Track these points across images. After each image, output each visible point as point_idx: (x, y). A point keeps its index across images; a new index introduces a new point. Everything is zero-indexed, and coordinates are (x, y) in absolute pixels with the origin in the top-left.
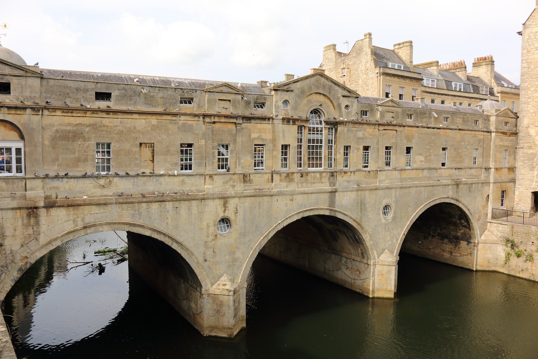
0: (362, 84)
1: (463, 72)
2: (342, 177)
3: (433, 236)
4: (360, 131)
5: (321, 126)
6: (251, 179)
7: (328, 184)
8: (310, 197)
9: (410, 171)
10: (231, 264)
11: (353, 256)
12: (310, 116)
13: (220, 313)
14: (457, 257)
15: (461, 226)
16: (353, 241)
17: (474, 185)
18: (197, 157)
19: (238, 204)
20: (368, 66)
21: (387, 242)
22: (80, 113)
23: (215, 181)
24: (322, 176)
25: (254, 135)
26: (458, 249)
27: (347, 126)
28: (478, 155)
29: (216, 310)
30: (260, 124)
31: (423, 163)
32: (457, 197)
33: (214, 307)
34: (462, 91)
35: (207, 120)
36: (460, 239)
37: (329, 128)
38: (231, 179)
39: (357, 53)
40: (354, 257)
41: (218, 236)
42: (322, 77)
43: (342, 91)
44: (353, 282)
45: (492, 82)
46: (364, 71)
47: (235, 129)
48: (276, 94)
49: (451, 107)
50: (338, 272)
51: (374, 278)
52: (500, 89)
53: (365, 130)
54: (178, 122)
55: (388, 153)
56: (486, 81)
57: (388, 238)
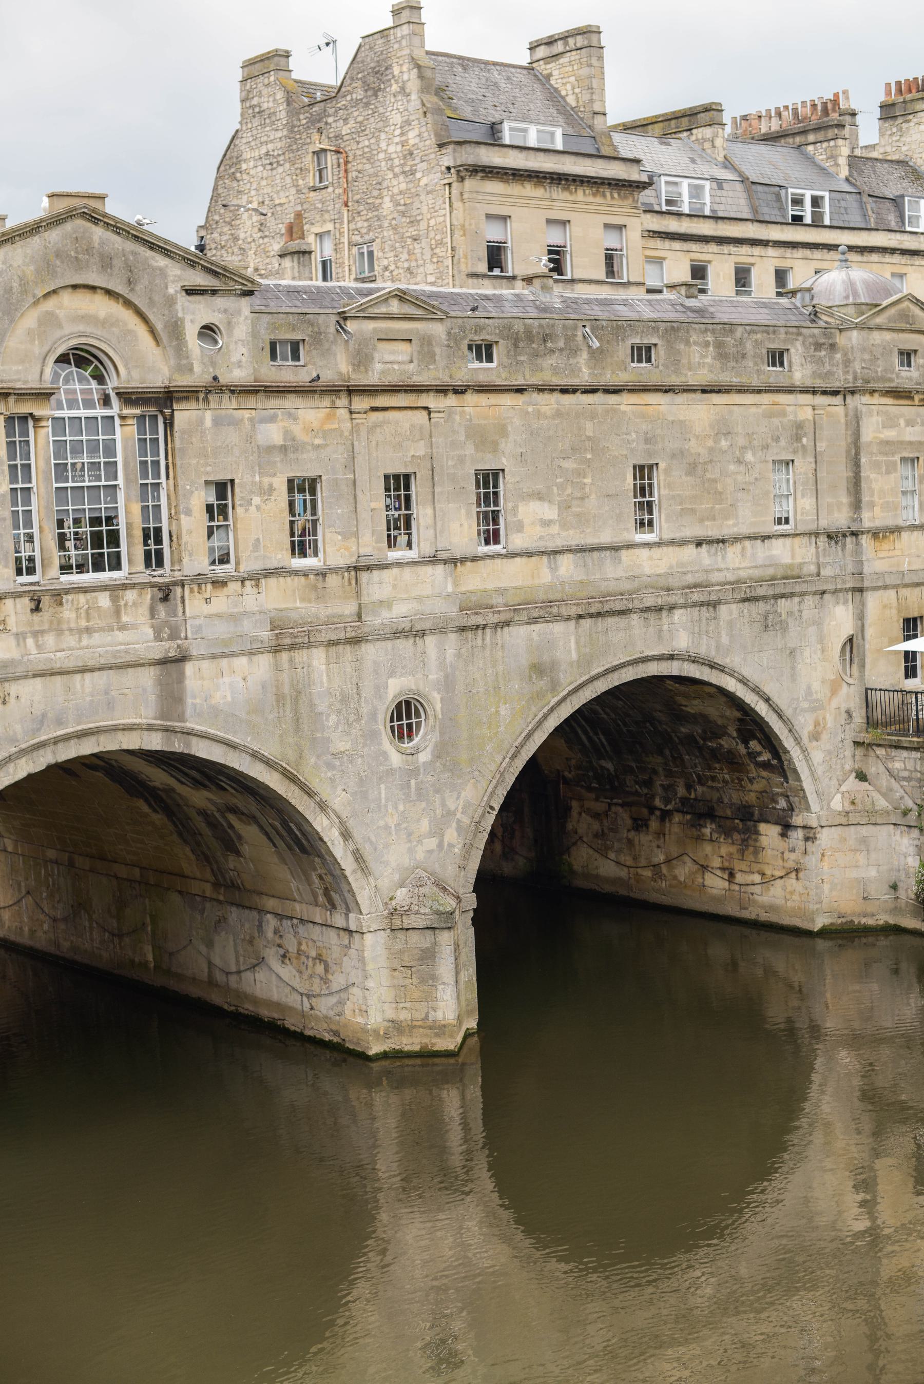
0: (396, 215)
2: (208, 601)
3: (665, 815)
4: (272, 419)
5: (107, 412)
7: (150, 632)
8: (78, 686)
9: (498, 561)
11: (297, 907)
12: (56, 375)
14: (751, 889)
15: (752, 766)
17: (781, 602)
20: (411, 142)
21: (420, 842)
24: (122, 603)
27: (212, 406)
28: (795, 483)
31: (555, 529)
32: (713, 653)
34: (827, 222)
36: (756, 817)
37: (141, 418)
39: (367, 87)
40: (301, 911)
42: (96, 224)
43: (182, 269)
46: (396, 162)
50: (256, 975)
53: (290, 415)
57: (425, 825)
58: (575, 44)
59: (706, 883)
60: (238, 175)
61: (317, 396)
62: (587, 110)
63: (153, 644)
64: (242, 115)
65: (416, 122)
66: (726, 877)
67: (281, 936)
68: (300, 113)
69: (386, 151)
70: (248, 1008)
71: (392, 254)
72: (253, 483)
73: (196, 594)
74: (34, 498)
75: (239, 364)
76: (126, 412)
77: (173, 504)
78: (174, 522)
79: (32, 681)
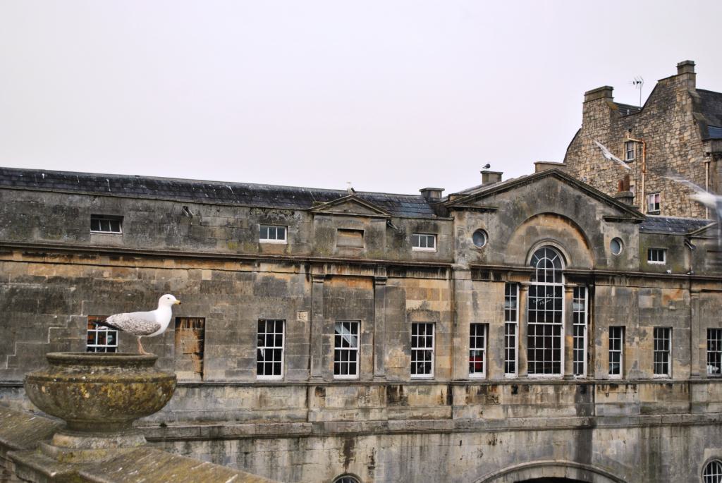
2: (607, 395)
4: (648, 293)
8: (534, 438)
18: (292, 349)
19: (376, 449)
20: (686, 138)
22: (59, 256)
24: (561, 392)
25: (412, 304)
27: (616, 284)
35: (315, 272)
37: (576, 289)
38: (361, 395)
39: (659, 107)
42: (560, 180)
46: (676, 149)
47: (372, 291)
54: (255, 276)
60: (579, 153)
61: (672, 281)
63: (576, 417)
64: (583, 121)
69: (669, 143)
71: (671, 200)
72: (636, 329)
73: (601, 390)
74: (517, 330)
75: (632, 262)
76: (569, 284)
77: (591, 338)
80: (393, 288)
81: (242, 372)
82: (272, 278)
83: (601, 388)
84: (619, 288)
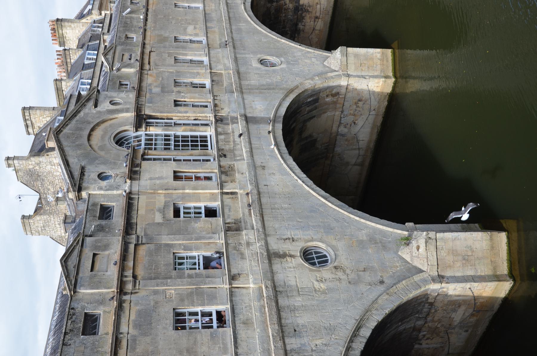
1: (71, 53)
4: (151, 90)
6: (233, 221)
7: (235, 125)
10: (380, 245)
13: (468, 256)
16: (316, 108)
18: (200, 302)
19: (278, 237)
21: (313, 62)
23: (241, 271)
24: (223, 132)
25: (158, 218)
26: (311, 8)
27: (144, 103)
29: (464, 262)
30: (139, 211)
31: (198, 26)
33: (459, 267)
35: (129, 287)
38: (235, 248)
39: (36, 180)
41: (336, 264)
42: (62, 131)
44: (373, 113)
45: (87, 21)
48: (87, 188)
49: (117, 7)
51: (367, 76)
52: (95, 12)
54: (132, 336)
55: (185, 62)
56: (84, 29)
58: (28, 116)
59: (319, 29)
62: (52, 113)
65: (50, 159)
66: (317, 20)
67: (347, 124)
68: (45, 209)
70: (372, 145)
78: (190, 118)
79: (255, 159)
80: (145, 231)
81: (223, 340)
82: (134, 321)
83: (218, 112)
84: (146, 102)
